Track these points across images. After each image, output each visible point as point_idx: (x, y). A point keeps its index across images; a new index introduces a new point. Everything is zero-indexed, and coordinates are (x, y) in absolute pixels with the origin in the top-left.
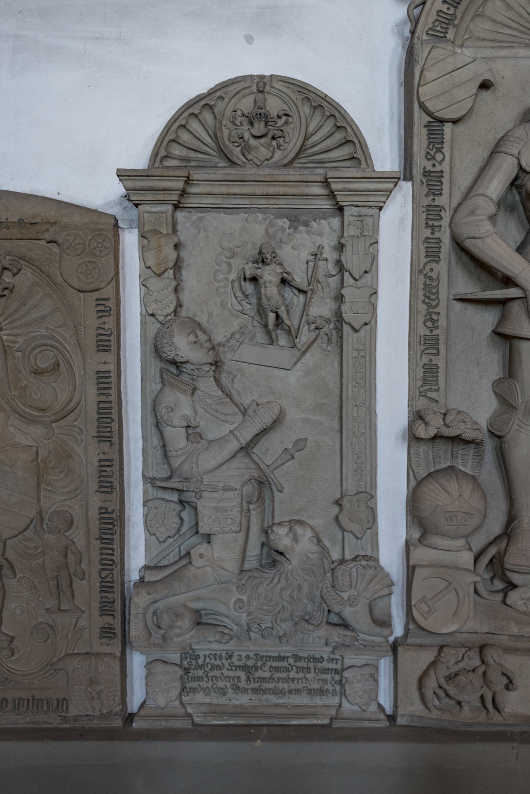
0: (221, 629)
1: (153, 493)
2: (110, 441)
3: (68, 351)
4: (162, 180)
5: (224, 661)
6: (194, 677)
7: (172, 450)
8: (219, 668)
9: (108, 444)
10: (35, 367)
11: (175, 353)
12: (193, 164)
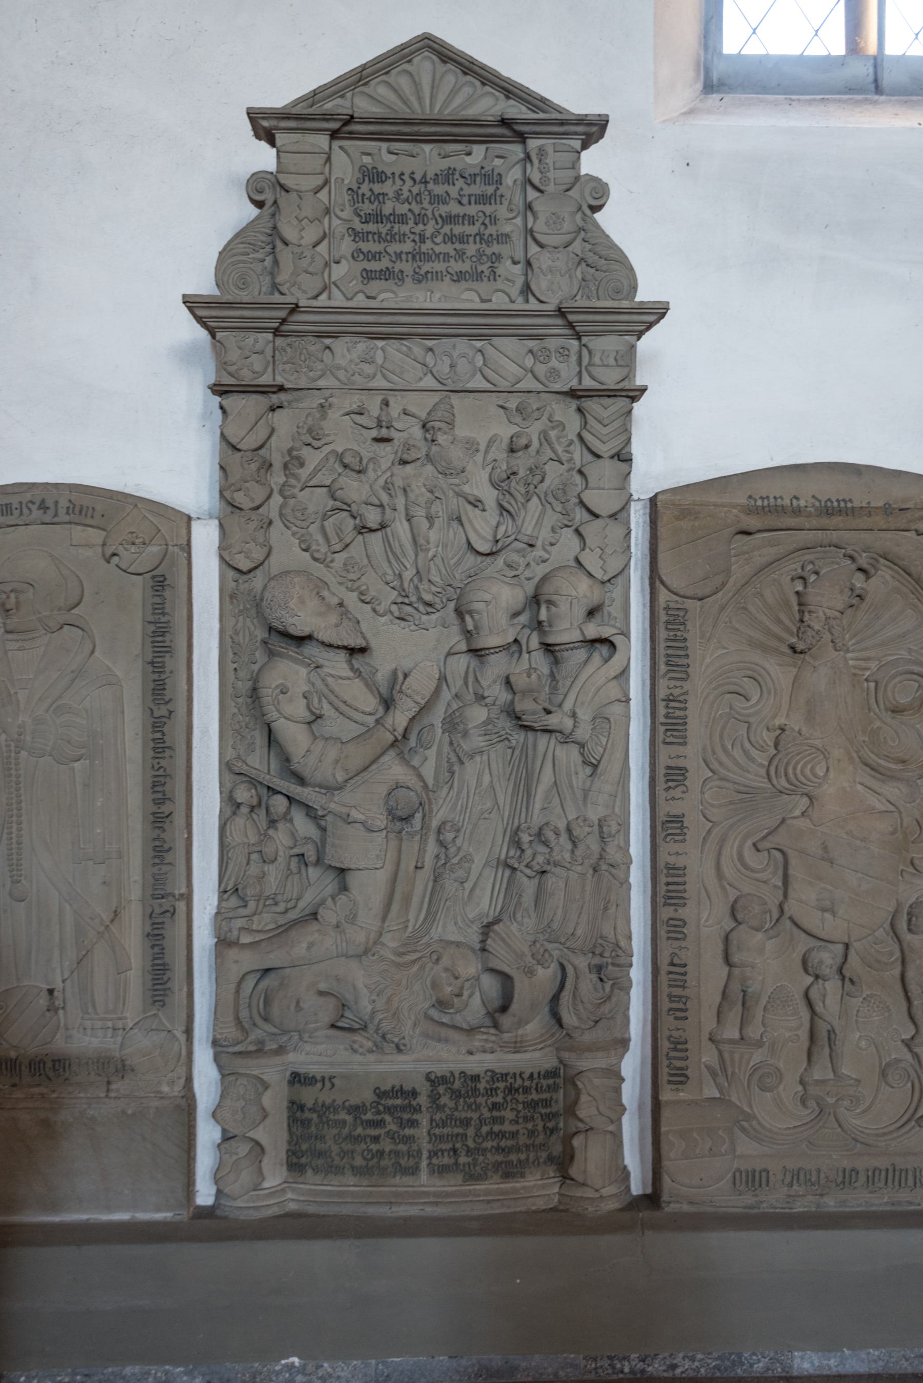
10: (894, 703)
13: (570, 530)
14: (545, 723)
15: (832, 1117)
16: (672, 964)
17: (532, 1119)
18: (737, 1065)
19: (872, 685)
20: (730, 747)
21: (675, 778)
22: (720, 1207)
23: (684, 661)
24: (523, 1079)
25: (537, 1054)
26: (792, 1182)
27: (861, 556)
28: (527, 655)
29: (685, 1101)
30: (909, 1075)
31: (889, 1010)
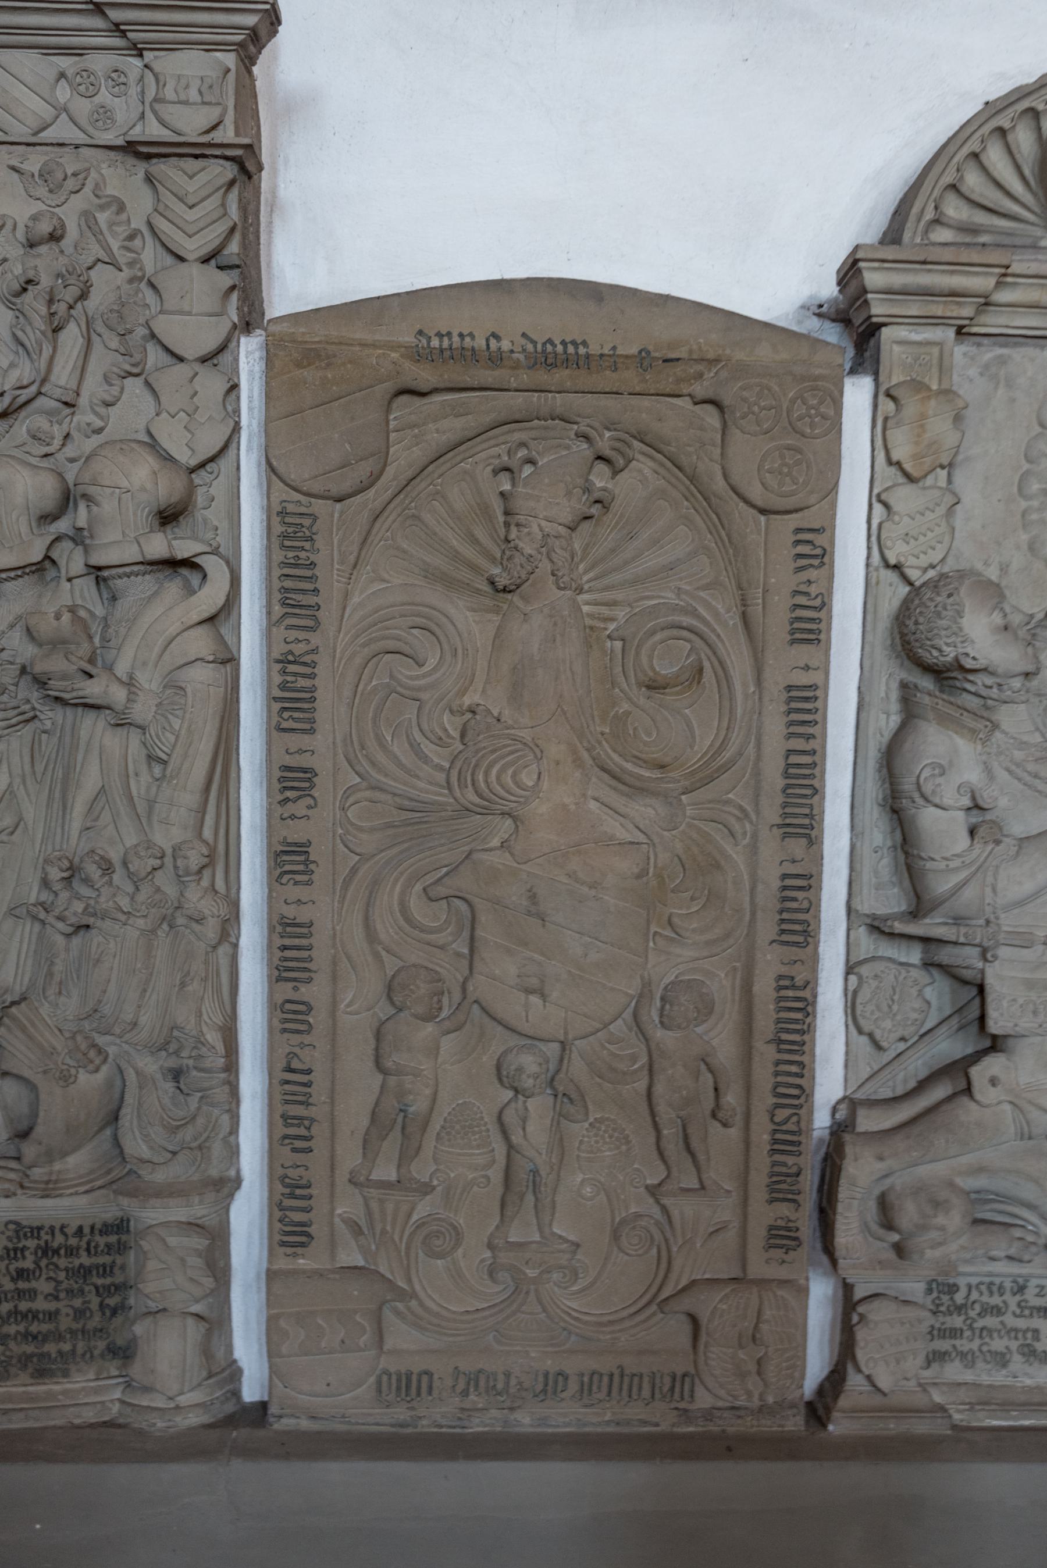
0: (1018, 1233)
1: (866, 944)
2: (808, 836)
3: (722, 641)
4: (952, 272)
5: (1007, 1297)
6: (945, 1330)
7: (937, 857)
8: (997, 1311)
9: (804, 841)
10: (651, 674)
11: (961, 650)
12: (983, 239)
13: (139, 382)
14: (81, 693)
15: (532, 1296)
16: (289, 1070)
17: (82, 1291)
18: (389, 1219)
19: (618, 644)
20: (389, 739)
21: (296, 784)
22: (358, 1424)
23: (312, 600)
24: (66, 1235)
25: (83, 1201)
26: (468, 1389)
27: (601, 436)
28: (68, 584)
29: (304, 1272)
30: (652, 1237)
31: (628, 1142)
